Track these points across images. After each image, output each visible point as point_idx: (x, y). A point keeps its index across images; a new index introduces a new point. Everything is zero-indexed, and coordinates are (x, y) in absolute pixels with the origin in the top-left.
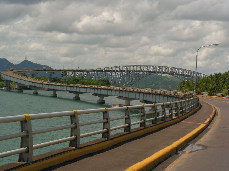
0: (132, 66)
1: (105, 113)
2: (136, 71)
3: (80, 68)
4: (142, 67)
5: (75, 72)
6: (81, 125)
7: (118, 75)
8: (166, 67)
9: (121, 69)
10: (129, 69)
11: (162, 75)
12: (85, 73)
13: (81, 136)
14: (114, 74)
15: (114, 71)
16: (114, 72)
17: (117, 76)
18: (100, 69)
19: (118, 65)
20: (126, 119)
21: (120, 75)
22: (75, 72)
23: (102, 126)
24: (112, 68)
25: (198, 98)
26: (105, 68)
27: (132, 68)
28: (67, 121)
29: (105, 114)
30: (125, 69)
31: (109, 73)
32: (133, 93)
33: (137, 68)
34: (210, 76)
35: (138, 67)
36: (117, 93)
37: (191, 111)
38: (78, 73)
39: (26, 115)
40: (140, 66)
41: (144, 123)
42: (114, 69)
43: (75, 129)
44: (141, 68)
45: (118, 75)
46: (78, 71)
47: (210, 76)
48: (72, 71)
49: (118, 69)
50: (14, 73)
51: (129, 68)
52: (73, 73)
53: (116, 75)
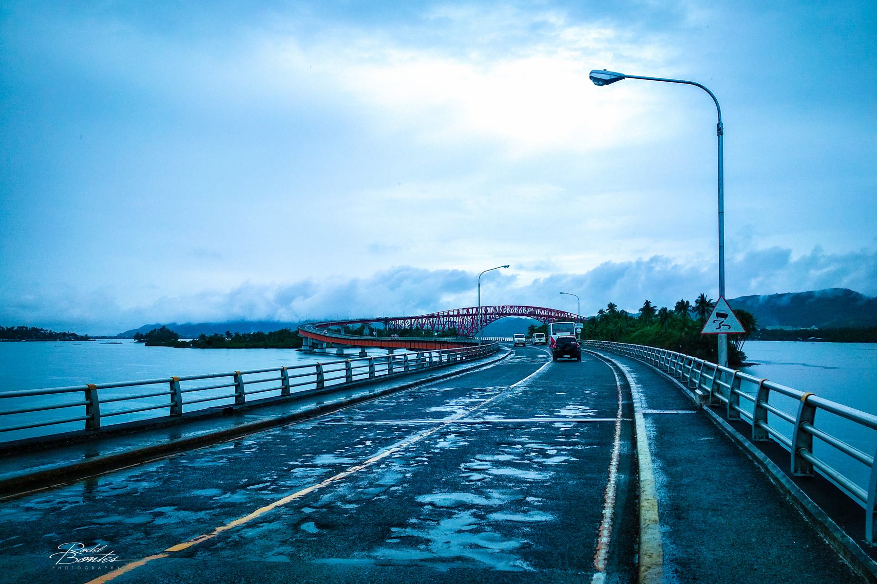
1: (347, 362)
4: (488, 309)
6: (102, 416)
7: (457, 321)
9: (461, 313)
10: (471, 313)
12: (424, 321)
14: (452, 320)
16: (451, 318)
17: (456, 322)
29: (347, 364)
32: (432, 344)
34: (598, 548)
35: (483, 309)
36: (408, 344)
37: (440, 366)
38: (414, 321)
42: (451, 313)
44: (487, 310)
45: (457, 321)
47: (598, 548)
50: (315, 327)
51: (470, 311)
52: (396, 322)
53: (455, 321)
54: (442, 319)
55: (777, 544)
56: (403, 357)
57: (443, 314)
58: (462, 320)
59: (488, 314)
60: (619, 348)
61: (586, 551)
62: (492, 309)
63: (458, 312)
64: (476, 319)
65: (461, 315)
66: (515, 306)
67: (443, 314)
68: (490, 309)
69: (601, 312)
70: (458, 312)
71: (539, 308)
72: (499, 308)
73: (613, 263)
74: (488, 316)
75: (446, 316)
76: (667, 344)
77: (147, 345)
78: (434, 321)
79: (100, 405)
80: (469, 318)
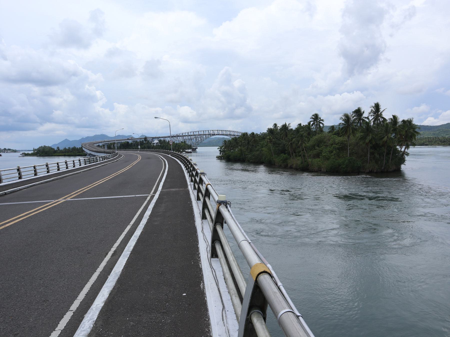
2: (200, 135)
4: (209, 131)
8: (222, 130)
15: (184, 136)
24: (188, 133)
27: (197, 133)
30: (192, 134)
33: (199, 133)
42: (184, 135)
75: (181, 136)
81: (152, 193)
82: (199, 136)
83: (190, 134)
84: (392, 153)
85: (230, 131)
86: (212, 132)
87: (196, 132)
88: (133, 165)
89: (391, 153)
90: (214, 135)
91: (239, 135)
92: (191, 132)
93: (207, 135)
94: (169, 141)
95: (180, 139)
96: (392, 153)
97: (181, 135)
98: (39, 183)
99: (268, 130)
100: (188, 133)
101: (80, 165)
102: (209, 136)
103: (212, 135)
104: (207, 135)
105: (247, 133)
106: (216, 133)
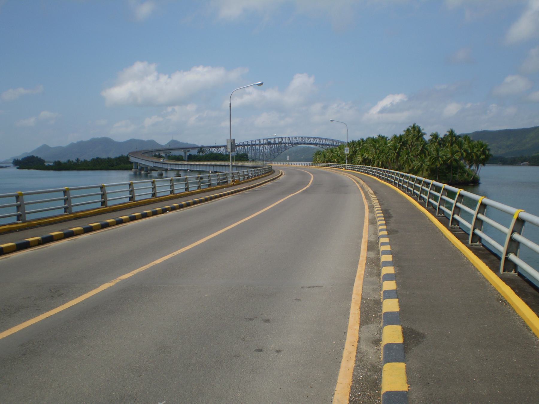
0: (272, 138)
3: (217, 145)
4: (291, 139)
5: (212, 148)
11: (312, 147)
13: (26, 212)
15: (254, 145)
16: (254, 146)
18: (239, 144)
19: (267, 137)
20: (171, 186)
21: (260, 149)
22: (212, 148)
23: (170, 187)
24: (260, 140)
25: (272, 167)
26: (240, 143)
28: (13, 201)
31: (257, 146)
33: (275, 141)
35: (287, 139)
39: (102, 184)
40: (289, 138)
41: (244, 178)
42: (254, 143)
43: (132, 192)
44: (282, 140)
46: (215, 148)
48: (209, 148)
49: (258, 142)
54: (246, 147)
55: (102, 389)
56: (242, 173)
57: (247, 143)
58: (262, 148)
59: (283, 144)
60: (369, 171)
61: (189, 370)
62: (293, 139)
63: (260, 141)
64: (274, 147)
65: (262, 144)
66: (305, 137)
67: (247, 143)
68: (292, 139)
69: (373, 137)
70: (260, 141)
71: (324, 139)
72: (292, 139)
73: (83, 160)
74: (283, 145)
75: (249, 145)
76: (396, 167)
77: (18, 168)
78: (249, 149)
79: (108, 201)
80: (268, 147)
81: (432, 182)
82: (276, 145)
83: (262, 142)
84: (382, 317)
85: (327, 139)
86: (293, 141)
87: (271, 139)
88: (139, 202)
89: (382, 317)
90: (298, 143)
91: (334, 144)
92: (264, 139)
93: (287, 143)
94: (237, 154)
95: (239, 149)
96: (382, 317)
97: (250, 143)
98: (39, 223)
99: (352, 141)
100: (260, 140)
101: (229, 172)
102: (290, 145)
103: (295, 144)
104: (287, 143)
105: (382, 138)
106: (300, 140)
